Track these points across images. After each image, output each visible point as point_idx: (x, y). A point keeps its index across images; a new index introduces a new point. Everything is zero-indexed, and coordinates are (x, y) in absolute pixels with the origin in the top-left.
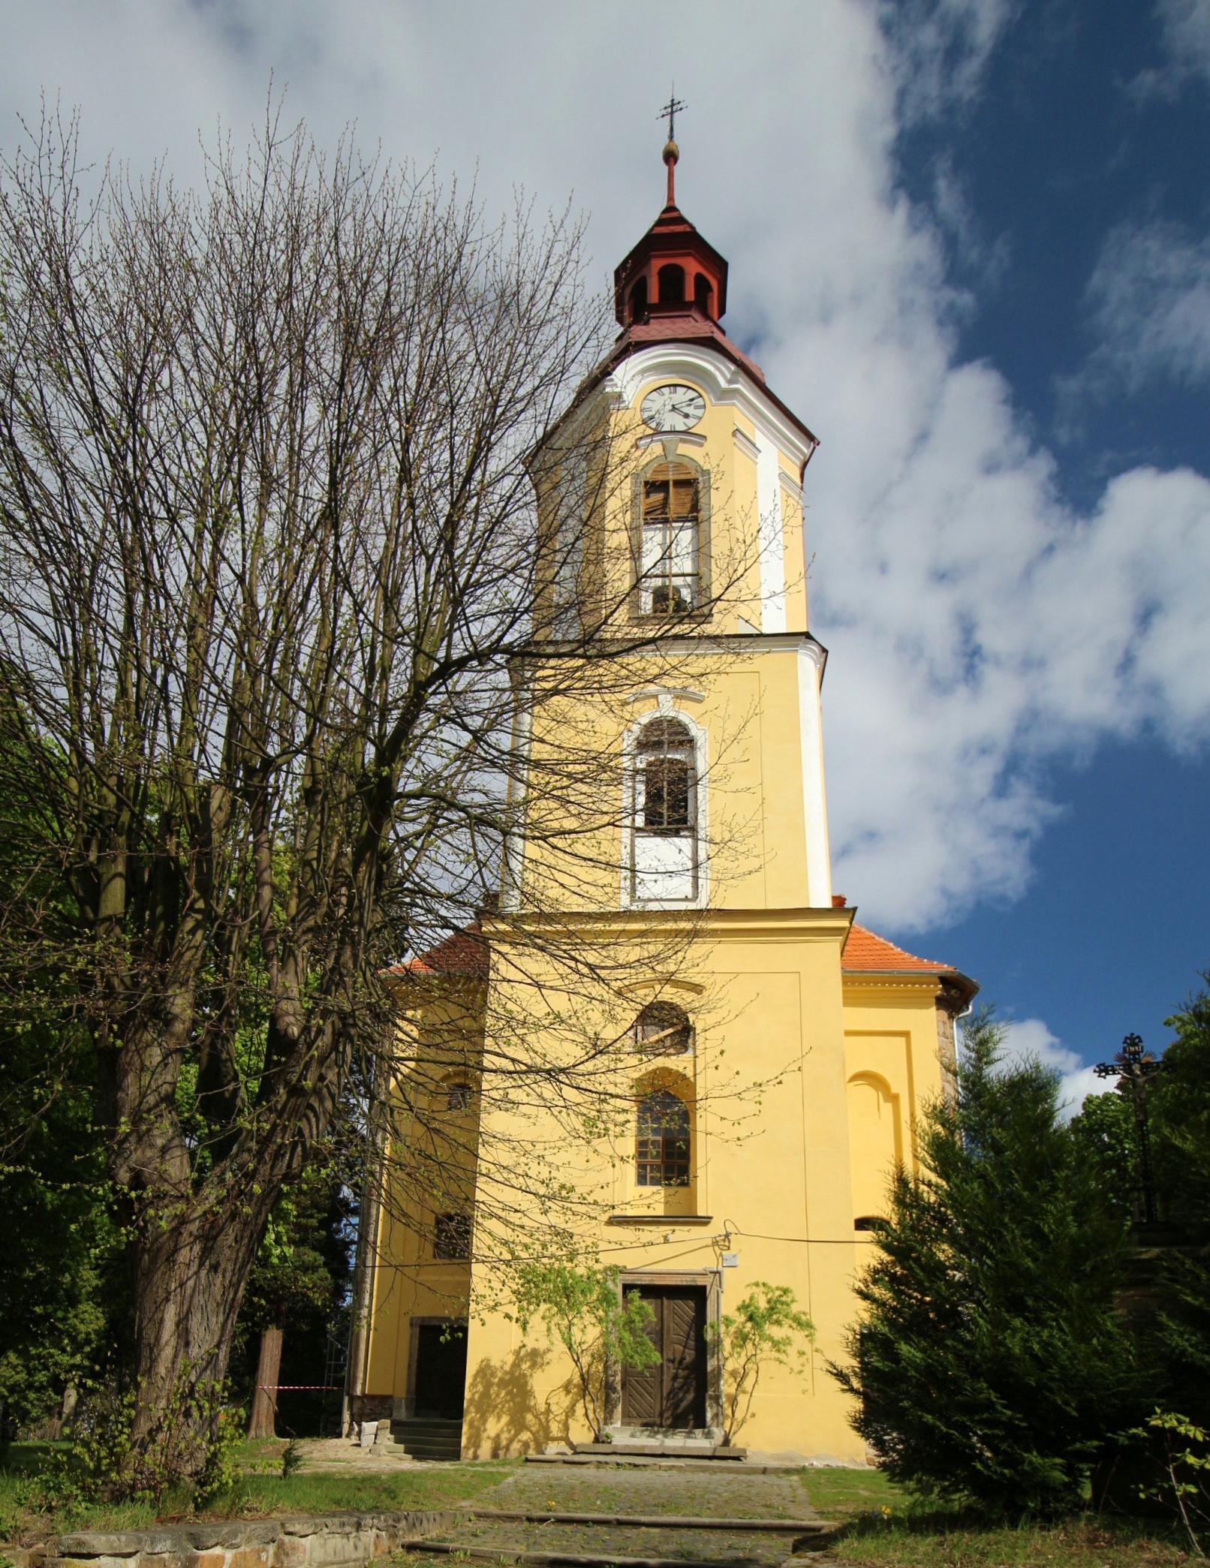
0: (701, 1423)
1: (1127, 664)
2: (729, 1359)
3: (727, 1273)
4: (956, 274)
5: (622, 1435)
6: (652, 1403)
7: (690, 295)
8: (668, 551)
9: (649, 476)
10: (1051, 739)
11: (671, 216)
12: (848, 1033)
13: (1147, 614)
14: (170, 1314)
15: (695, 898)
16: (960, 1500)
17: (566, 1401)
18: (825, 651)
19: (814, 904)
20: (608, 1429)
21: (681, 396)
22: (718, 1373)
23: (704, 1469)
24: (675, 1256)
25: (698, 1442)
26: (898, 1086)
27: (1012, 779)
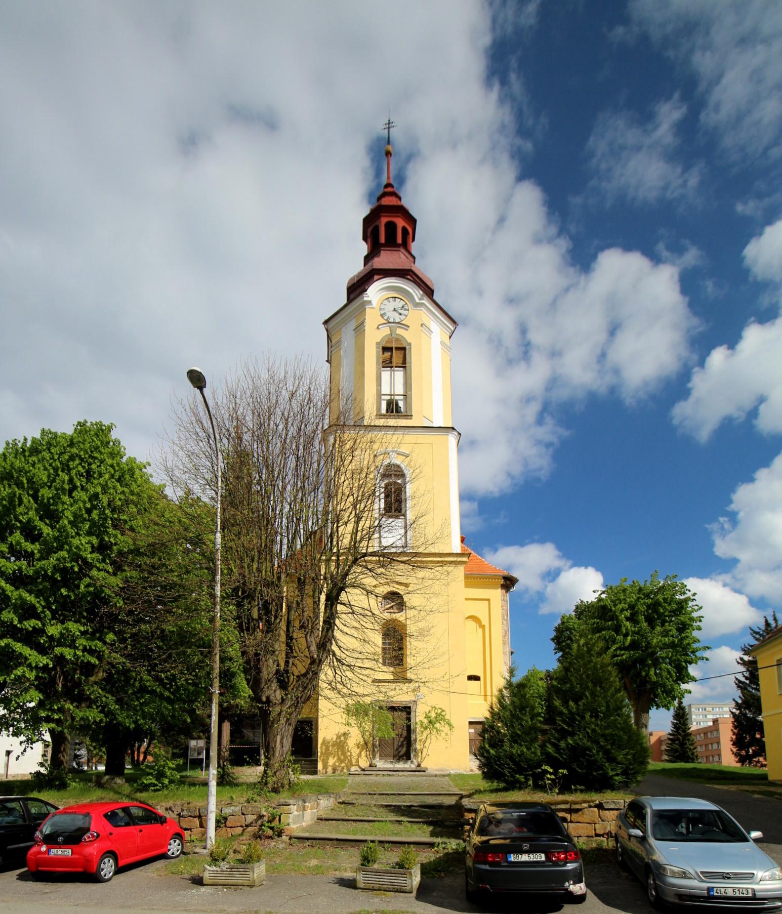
0: (409, 758)
1: (603, 356)
2: (419, 736)
4: (522, 131)
5: (381, 764)
6: (390, 751)
7: (399, 240)
8: (393, 382)
9: (384, 345)
10: (562, 394)
12: (466, 599)
13: (613, 330)
16: (502, 785)
17: (358, 751)
18: (460, 434)
19: (455, 552)
20: (374, 762)
21: (398, 304)
22: (415, 740)
23: (414, 776)
24: (401, 695)
25: (408, 765)
26: (485, 622)
27: (545, 414)
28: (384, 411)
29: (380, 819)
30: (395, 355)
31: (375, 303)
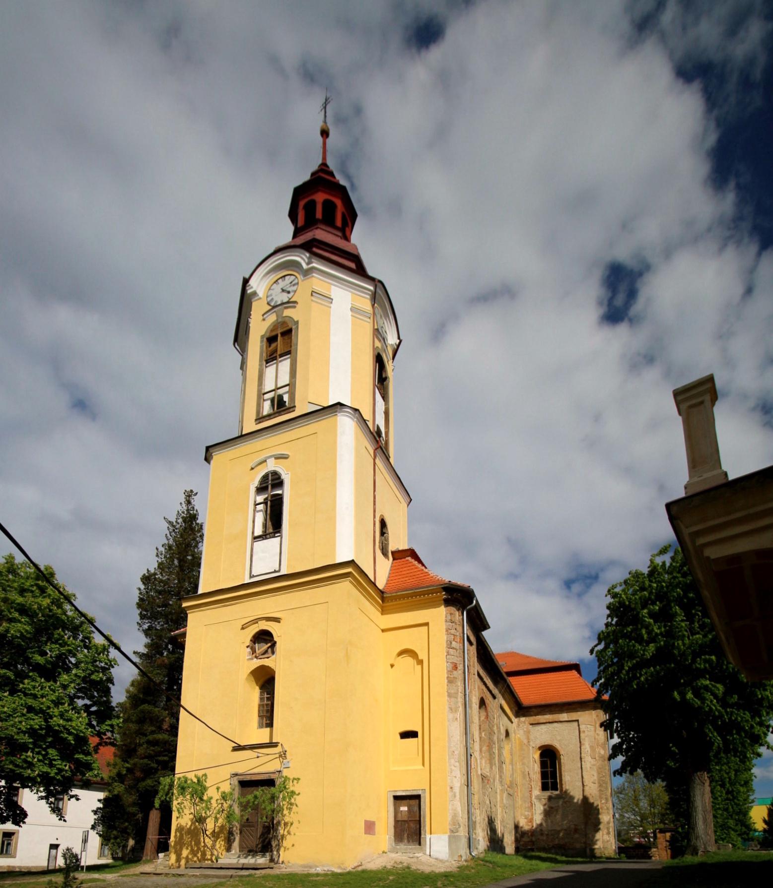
9: (268, 335)
11: (324, 168)
12: (383, 631)
15: (279, 571)
22: (279, 823)
26: (422, 655)
28: (267, 408)
29: (475, 800)
30: (281, 342)
31: (261, 293)
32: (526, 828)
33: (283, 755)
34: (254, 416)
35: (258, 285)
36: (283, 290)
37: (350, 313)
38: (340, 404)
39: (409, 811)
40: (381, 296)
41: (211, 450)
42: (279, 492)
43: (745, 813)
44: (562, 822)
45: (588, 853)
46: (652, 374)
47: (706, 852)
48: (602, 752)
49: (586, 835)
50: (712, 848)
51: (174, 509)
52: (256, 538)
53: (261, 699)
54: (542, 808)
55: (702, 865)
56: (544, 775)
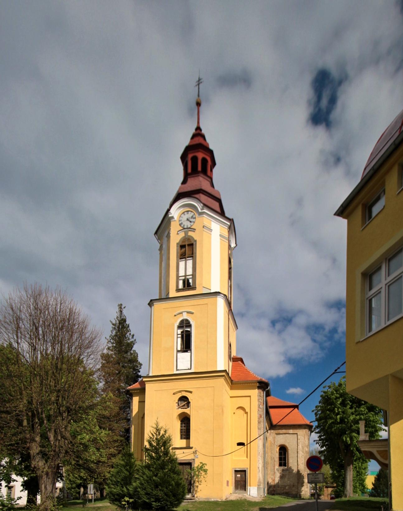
3: (196, 459)
8: (185, 268)
9: (181, 244)
12: (231, 397)
14: (43, 486)
15: (191, 369)
28: (181, 286)
30: (188, 249)
31: (176, 217)
32: (272, 484)
33: (195, 452)
34: (175, 288)
35: (175, 212)
36: (188, 220)
37: (219, 237)
38: (219, 292)
39: (241, 476)
40: (232, 228)
41: (153, 301)
42: (189, 329)
43: (364, 480)
44: (287, 482)
45: (297, 496)
46: (339, 172)
47: (350, 496)
48: (307, 450)
49: (298, 488)
50: (351, 495)
51: (113, 315)
52: (178, 351)
53: (181, 427)
54: (279, 475)
55: (348, 501)
56: (280, 459)
